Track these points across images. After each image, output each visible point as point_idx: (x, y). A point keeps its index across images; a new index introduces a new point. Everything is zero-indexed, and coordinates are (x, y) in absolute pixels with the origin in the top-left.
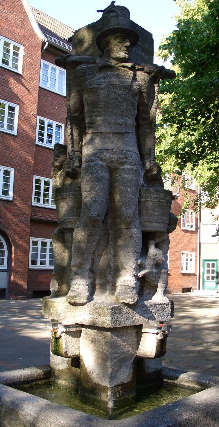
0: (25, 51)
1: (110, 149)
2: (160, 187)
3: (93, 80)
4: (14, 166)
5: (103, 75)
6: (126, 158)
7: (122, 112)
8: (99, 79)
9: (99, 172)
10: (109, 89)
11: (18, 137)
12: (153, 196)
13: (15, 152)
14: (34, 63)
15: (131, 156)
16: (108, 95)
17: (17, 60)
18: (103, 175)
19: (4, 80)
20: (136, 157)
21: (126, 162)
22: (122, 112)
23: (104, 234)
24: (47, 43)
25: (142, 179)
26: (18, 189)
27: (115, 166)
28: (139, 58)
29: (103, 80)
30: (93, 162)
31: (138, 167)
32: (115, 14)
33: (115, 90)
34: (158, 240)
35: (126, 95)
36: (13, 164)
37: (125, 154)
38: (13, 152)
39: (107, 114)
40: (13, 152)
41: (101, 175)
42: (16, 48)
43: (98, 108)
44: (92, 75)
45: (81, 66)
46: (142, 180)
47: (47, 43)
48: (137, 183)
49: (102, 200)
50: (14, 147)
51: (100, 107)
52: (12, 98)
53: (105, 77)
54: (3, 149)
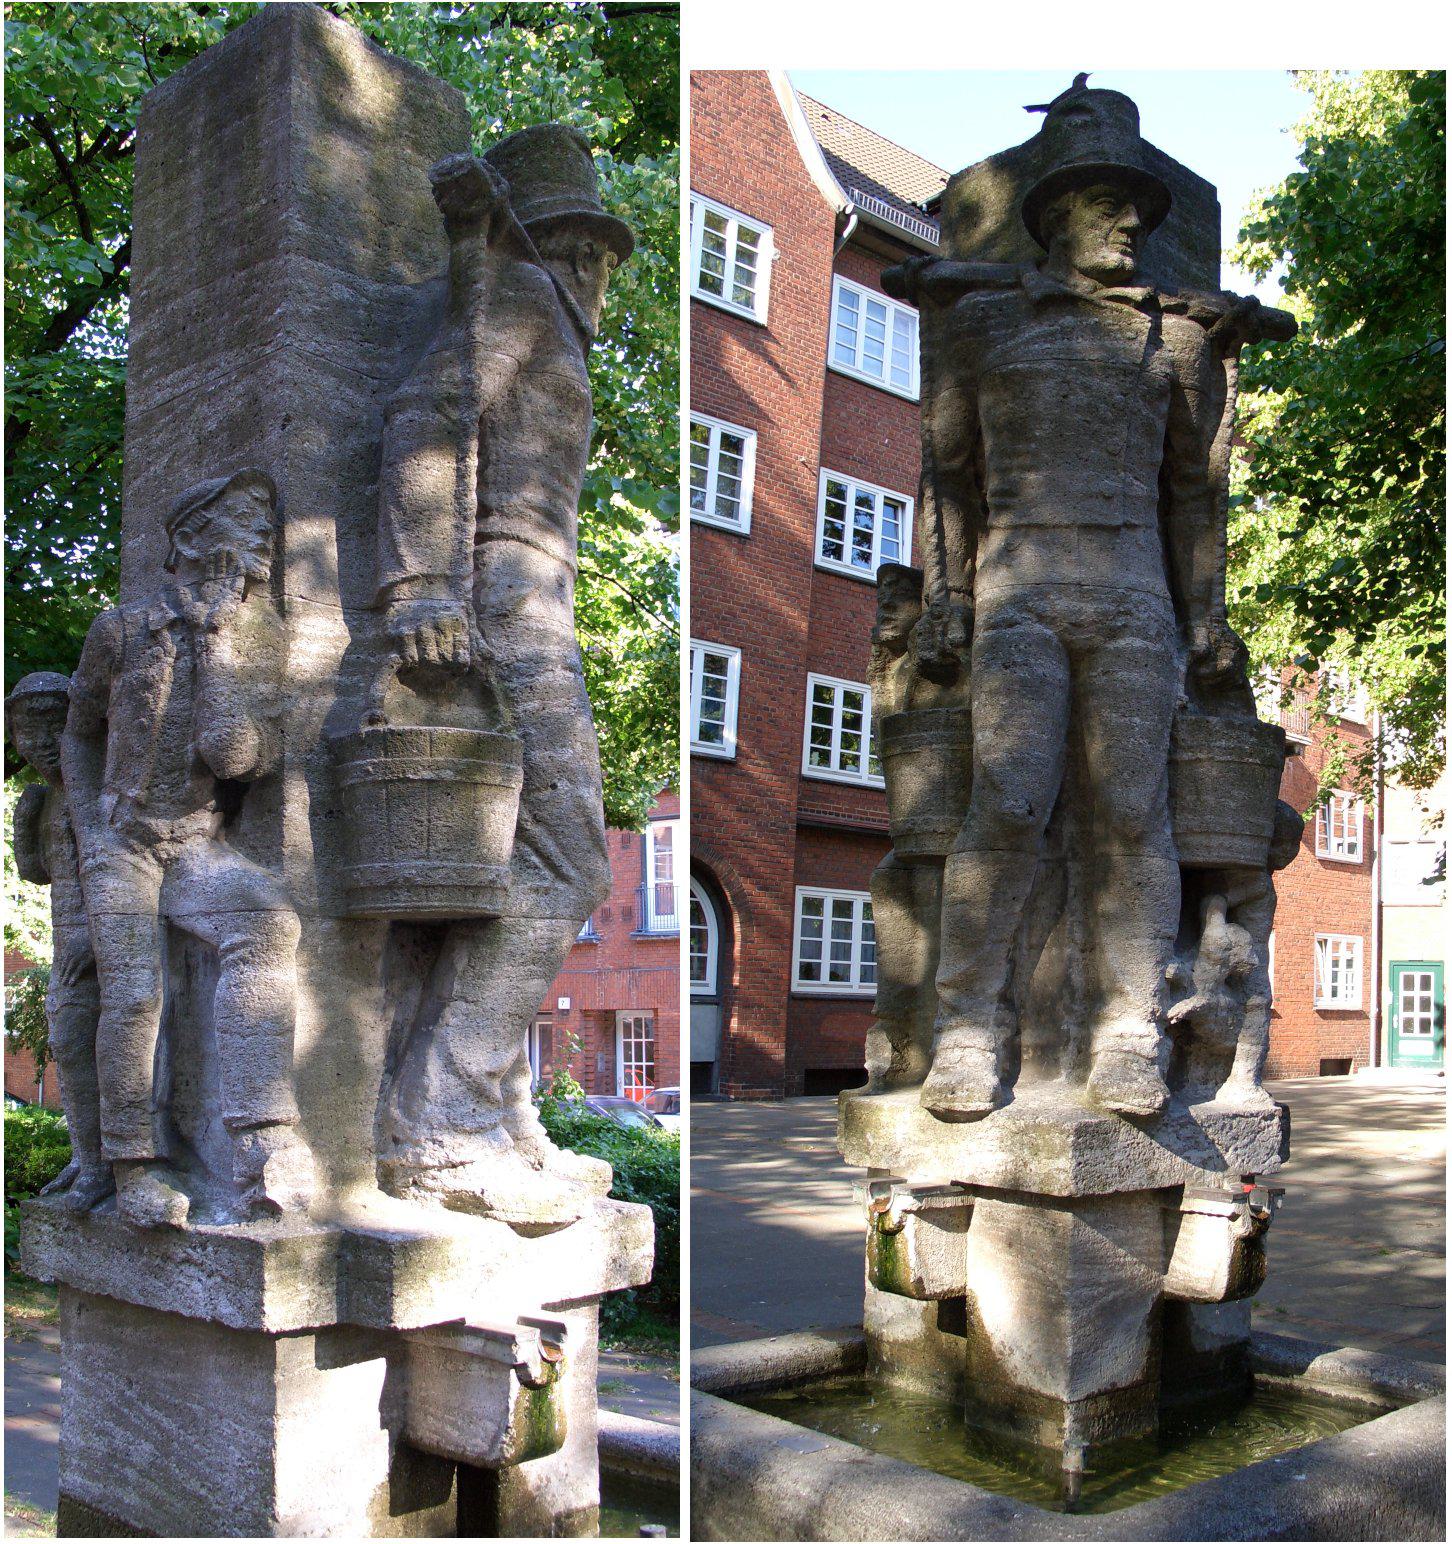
0: (777, 244)
6: (1128, 613)
8: (1033, 340)
15: (1142, 608)
16: (1065, 397)
17: (749, 277)
18: (1046, 671)
21: (1125, 626)
24: (854, 219)
28: (1170, 270)
30: (1011, 626)
32: (1088, 118)
34: (1235, 897)
37: (1121, 600)
39: (1059, 461)
41: (1040, 671)
42: (748, 236)
43: (1029, 440)
47: (854, 219)
53: (1052, 334)
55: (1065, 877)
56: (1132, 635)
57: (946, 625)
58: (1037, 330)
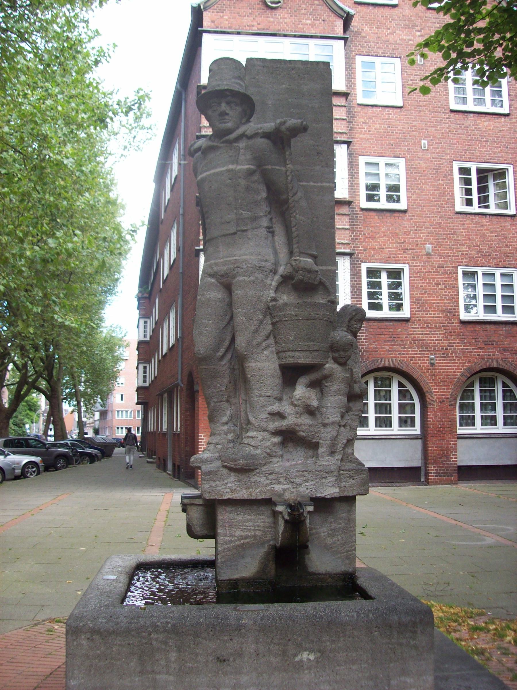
6: (238, 267)
34: (314, 376)
41: (208, 297)
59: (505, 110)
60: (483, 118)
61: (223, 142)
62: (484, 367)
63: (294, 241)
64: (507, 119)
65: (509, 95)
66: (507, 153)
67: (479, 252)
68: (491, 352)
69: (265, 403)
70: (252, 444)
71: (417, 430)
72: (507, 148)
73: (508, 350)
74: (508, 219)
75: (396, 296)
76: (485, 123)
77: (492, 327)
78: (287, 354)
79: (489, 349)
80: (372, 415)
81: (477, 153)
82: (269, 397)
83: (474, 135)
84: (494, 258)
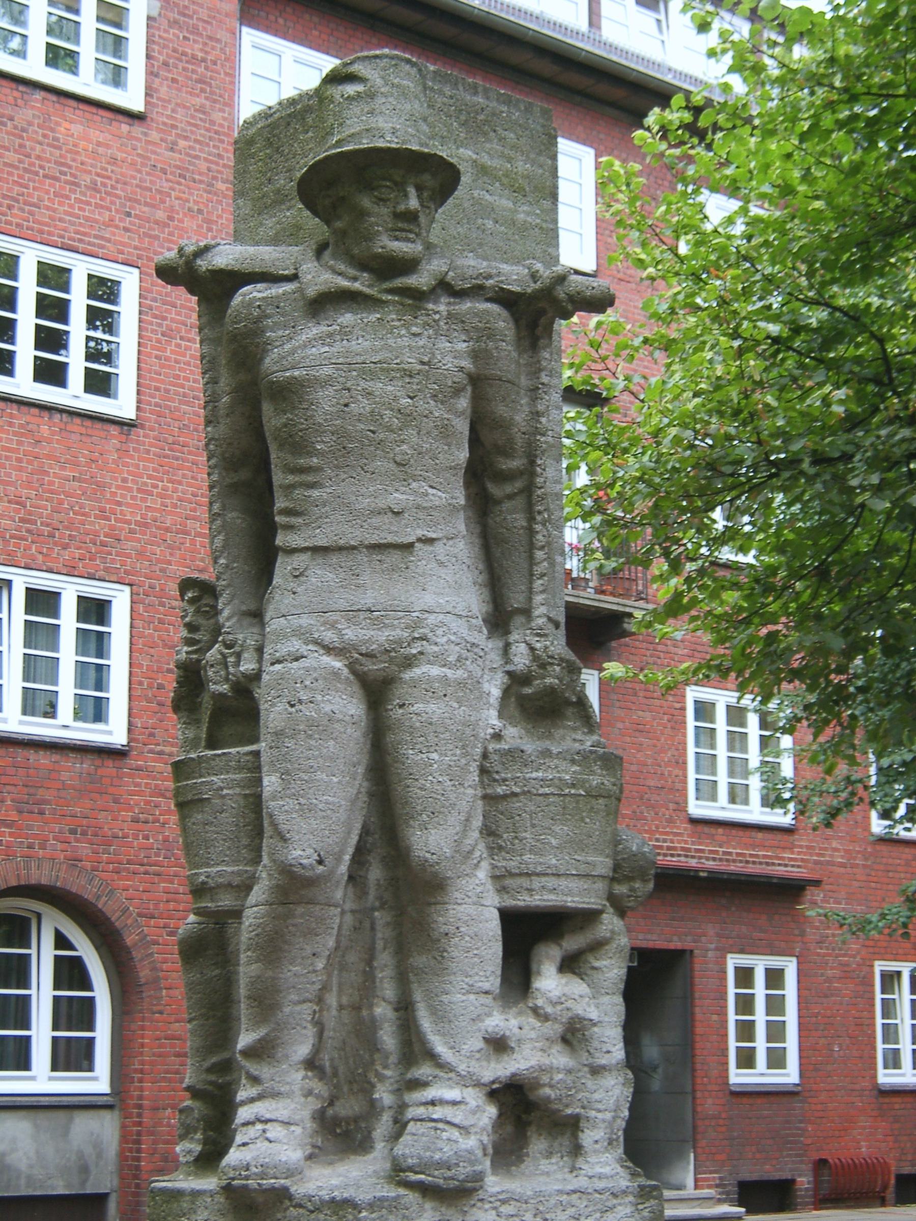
1: (359, 610)
2: (584, 733)
3: (287, 347)
4: (126, 572)
5: (325, 328)
6: (423, 638)
7: (398, 464)
8: (309, 343)
9: (319, 698)
10: (349, 385)
11: (142, 427)
12: (534, 775)
13: (128, 505)
14: (207, 53)
15: (440, 632)
16: (346, 405)
17: (118, 45)
18: (335, 708)
19: (60, 148)
20: (464, 632)
21: (421, 653)
22: (398, 464)
23: (357, 925)
25: (494, 713)
26: (150, 686)
27: (383, 669)
28: (489, 224)
29: (327, 349)
30: (297, 659)
31: (471, 668)
32: (360, 88)
33: (371, 384)
34: (572, 943)
35: (411, 398)
36: (124, 564)
37: (417, 624)
38: (119, 504)
39: (344, 476)
40: (119, 504)
41: (328, 708)
43: (310, 454)
44: (285, 327)
45: (244, 295)
46: (492, 718)
48: (468, 731)
49: (333, 803)
50: (125, 480)
51: (320, 454)
52: (102, 238)
53: (330, 335)
54: (68, 495)
55: (373, 928)
56: (429, 662)
57: (238, 655)
58: (315, 332)
59: (132, 97)
60: (70, 110)
61: (391, 291)
62: (13, 883)
63: (538, 584)
64: (138, 130)
65: (148, 57)
66: (126, 229)
67: (22, 520)
68: (35, 836)
69: (480, 1010)
70: (456, 1121)
71: (98, 1081)
72: (129, 214)
73: (84, 833)
74: (114, 430)
75: (95, 676)
76: (74, 127)
77: (44, 759)
78: (536, 883)
79: (30, 828)
80: (42, 1033)
81: (43, 215)
82: (486, 993)
83: (39, 157)
84: (65, 547)
